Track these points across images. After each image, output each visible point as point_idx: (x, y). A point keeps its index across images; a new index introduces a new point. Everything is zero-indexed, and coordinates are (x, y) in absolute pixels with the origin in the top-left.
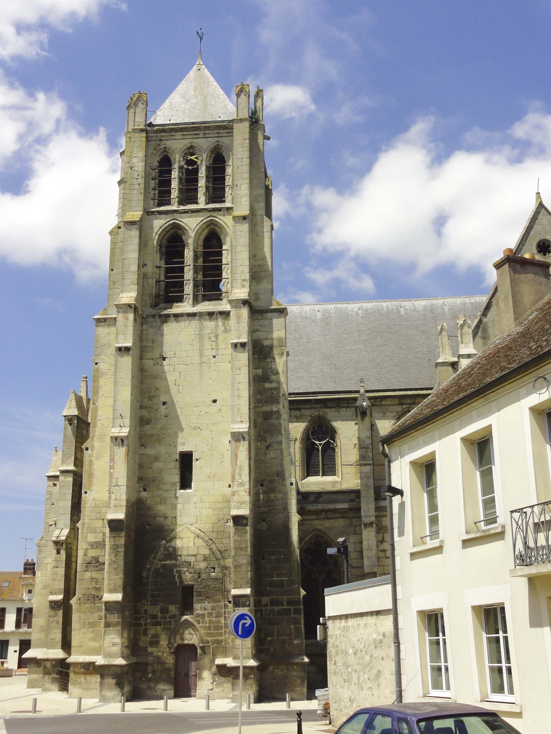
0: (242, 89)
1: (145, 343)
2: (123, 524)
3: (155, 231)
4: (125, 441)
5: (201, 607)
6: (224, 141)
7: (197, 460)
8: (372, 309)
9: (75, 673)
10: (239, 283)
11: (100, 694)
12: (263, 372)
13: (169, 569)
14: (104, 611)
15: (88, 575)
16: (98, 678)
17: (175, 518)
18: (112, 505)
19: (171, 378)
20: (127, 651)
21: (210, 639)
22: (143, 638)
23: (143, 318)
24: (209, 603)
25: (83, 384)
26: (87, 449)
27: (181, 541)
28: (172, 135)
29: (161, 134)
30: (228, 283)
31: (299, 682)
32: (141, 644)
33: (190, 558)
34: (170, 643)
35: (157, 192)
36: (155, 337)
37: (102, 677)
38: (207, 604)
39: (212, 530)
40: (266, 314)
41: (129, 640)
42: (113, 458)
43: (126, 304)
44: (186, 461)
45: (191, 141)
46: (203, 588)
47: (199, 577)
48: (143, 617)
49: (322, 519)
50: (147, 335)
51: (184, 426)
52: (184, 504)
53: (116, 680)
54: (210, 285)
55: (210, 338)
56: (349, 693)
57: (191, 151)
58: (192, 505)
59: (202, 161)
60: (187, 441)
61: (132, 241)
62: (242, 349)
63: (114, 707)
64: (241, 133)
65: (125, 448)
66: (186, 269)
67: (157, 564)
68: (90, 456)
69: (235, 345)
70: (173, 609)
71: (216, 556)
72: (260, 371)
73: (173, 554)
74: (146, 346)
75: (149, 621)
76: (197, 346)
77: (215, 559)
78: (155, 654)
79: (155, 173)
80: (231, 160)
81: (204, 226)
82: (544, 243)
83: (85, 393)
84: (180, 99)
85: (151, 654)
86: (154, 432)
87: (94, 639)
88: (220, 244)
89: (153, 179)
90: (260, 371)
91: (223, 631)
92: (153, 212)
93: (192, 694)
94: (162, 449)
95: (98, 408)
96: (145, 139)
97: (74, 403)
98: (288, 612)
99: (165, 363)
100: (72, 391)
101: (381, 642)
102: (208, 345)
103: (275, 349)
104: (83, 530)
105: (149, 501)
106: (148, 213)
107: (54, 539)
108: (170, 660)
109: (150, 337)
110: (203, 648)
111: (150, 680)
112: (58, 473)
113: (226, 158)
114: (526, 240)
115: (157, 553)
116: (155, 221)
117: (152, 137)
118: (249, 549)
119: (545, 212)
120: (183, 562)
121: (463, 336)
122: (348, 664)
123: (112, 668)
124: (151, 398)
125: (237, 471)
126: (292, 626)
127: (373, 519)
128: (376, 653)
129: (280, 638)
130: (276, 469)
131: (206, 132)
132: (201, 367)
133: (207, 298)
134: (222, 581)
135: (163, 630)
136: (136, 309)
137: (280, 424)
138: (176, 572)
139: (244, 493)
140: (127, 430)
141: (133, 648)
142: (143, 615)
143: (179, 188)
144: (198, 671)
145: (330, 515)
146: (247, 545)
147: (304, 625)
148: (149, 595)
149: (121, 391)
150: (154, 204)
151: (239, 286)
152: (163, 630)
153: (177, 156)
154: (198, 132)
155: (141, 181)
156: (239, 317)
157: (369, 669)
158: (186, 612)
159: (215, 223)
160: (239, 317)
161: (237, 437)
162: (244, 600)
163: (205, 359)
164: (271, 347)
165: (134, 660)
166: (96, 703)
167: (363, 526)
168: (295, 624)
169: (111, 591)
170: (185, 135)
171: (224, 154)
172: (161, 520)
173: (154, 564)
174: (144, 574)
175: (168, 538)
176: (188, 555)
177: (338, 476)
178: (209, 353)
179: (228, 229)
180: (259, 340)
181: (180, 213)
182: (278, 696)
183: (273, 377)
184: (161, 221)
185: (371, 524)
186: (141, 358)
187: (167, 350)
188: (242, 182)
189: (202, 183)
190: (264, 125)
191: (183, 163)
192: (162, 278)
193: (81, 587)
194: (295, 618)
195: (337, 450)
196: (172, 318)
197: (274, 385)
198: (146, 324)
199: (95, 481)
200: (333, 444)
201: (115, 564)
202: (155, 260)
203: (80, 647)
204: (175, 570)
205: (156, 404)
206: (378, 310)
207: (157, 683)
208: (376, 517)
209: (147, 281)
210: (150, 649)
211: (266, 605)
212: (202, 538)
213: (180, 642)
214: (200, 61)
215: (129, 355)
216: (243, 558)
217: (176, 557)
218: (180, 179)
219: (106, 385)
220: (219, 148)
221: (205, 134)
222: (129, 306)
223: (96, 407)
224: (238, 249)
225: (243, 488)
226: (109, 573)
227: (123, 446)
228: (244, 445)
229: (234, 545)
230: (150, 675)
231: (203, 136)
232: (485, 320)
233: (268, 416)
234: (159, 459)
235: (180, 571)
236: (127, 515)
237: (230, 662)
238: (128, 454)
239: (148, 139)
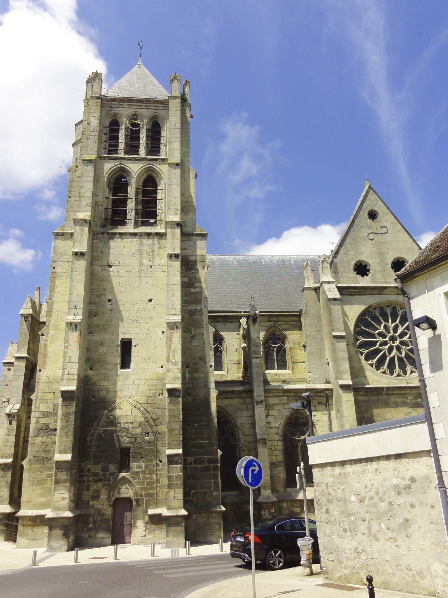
0: (175, 77)
1: (95, 254)
2: (74, 395)
3: (106, 171)
4: (78, 326)
6: (161, 113)
7: (136, 346)
8: (243, 260)
9: (23, 525)
10: (173, 211)
11: (48, 544)
12: (189, 280)
13: (111, 434)
14: (54, 470)
15: (39, 439)
16: (46, 530)
17: (116, 392)
18: (65, 379)
19: (115, 281)
20: (73, 505)
21: (143, 493)
22: (85, 493)
23: (94, 234)
24: (143, 462)
25: (37, 293)
26: (43, 335)
27: (120, 411)
28: (121, 105)
29: (113, 103)
30: (162, 214)
31: (217, 527)
32: (84, 498)
33: (128, 425)
35: (107, 144)
36: (103, 249)
37: (50, 529)
38: (141, 463)
39: (146, 402)
40: (191, 237)
41: (74, 494)
42: (68, 340)
43: (82, 220)
44: (126, 346)
45: (135, 110)
46: (139, 449)
47: (135, 441)
48: (86, 475)
49: (223, 398)
50: (97, 247)
51: (124, 320)
52: (124, 380)
53: (63, 531)
54: (148, 212)
55: (147, 253)
56: (354, 544)
57: (135, 117)
59: (143, 125)
60: (127, 331)
61: (88, 174)
62: (176, 259)
63: (64, 558)
64: (175, 106)
65: (78, 331)
66: (129, 201)
67: (100, 430)
69: (170, 256)
70: (113, 468)
71: (150, 424)
72: (187, 279)
73: (113, 422)
74: (96, 256)
75: (91, 478)
76: (137, 258)
77: (149, 426)
78: (96, 506)
79: (107, 130)
80: (166, 126)
81: (144, 171)
82: (372, 213)
83: (38, 299)
84: (126, 84)
85: (92, 507)
86: (100, 323)
87: (41, 495)
88: (155, 185)
89: (105, 134)
90: (187, 279)
91: (155, 486)
92: (105, 157)
93: (126, 540)
94: (107, 336)
96: (100, 104)
97: (29, 305)
98: (208, 469)
99: (110, 269)
100: (28, 295)
101: (409, 487)
102: (146, 258)
103: (198, 263)
104: (36, 400)
105: (94, 378)
106: (100, 157)
107: (7, 412)
108: (109, 511)
109: (99, 249)
110: (137, 501)
111: (90, 530)
112: (13, 360)
113: (161, 125)
114: (361, 209)
115: (100, 421)
116: (106, 164)
117: (105, 104)
118: (181, 416)
119: (373, 192)
120: (122, 428)
121: (324, 269)
122: (350, 512)
123: (61, 520)
124: (98, 296)
126: (212, 481)
127: (263, 398)
128: (400, 500)
129: (202, 490)
130: (199, 354)
131: (147, 104)
132: (140, 274)
133: (145, 223)
134: (154, 444)
135: (104, 486)
136: (90, 224)
137: (203, 320)
138: (116, 436)
139: (177, 371)
140: (81, 318)
141: (78, 502)
142: (86, 473)
143: (125, 143)
144: (133, 520)
145: (229, 395)
146: (180, 413)
147: (222, 479)
148: (92, 456)
150: (105, 152)
151: (173, 213)
152: (104, 486)
153: (125, 120)
154: (141, 104)
155: (96, 133)
156: (173, 235)
157: (389, 517)
158: (123, 470)
159: (153, 169)
160: (173, 235)
161: (172, 326)
162: (177, 458)
163: (143, 268)
164: (195, 262)
165: (78, 512)
166: (44, 552)
167: (255, 404)
168: (214, 479)
169: (61, 452)
170: (131, 105)
171: (160, 122)
172: (105, 393)
173: (97, 430)
174: (89, 439)
176: (127, 423)
177: (224, 371)
178: (147, 263)
179: (162, 175)
180: (186, 256)
181: (126, 160)
182: (200, 540)
183: (197, 284)
184: (111, 164)
185: (261, 402)
186: (92, 265)
187: (112, 259)
188: (175, 140)
189: (143, 140)
190: (190, 104)
191: (128, 125)
192: (110, 206)
193: (32, 450)
194: (214, 473)
195: (223, 352)
196: (118, 236)
197: (198, 290)
198: (97, 239)
200: (221, 348)
202: (105, 193)
203: (29, 502)
204: (115, 435)
205: (103, 301)
206: (247, 261)
207: (97, 532)
208: (265, 397)
210: (91, 503)
211: (191, 464)
213: (118, 496)
214: (140, 62)
215: (83, 259)
217: (116, 424)
218: (126, 136)
219: (62, 285)
220: (156, 117)
221: (146, 106)
222: (85, 221)
223: (52, 302)
224: (172, 187)
225: (176, 367)
226: (61, 436)
227: (76, 330)
228: (177, 333)
229: (169, 413)
230: (91, 525)
231: (145, 108)
232: (335, 260)
233: (192, 313)
234: (104, 343)
235: (119, 435)
236: (78, 387)
237: (165, 512)
238: (80, 337)
239: (102, 106)
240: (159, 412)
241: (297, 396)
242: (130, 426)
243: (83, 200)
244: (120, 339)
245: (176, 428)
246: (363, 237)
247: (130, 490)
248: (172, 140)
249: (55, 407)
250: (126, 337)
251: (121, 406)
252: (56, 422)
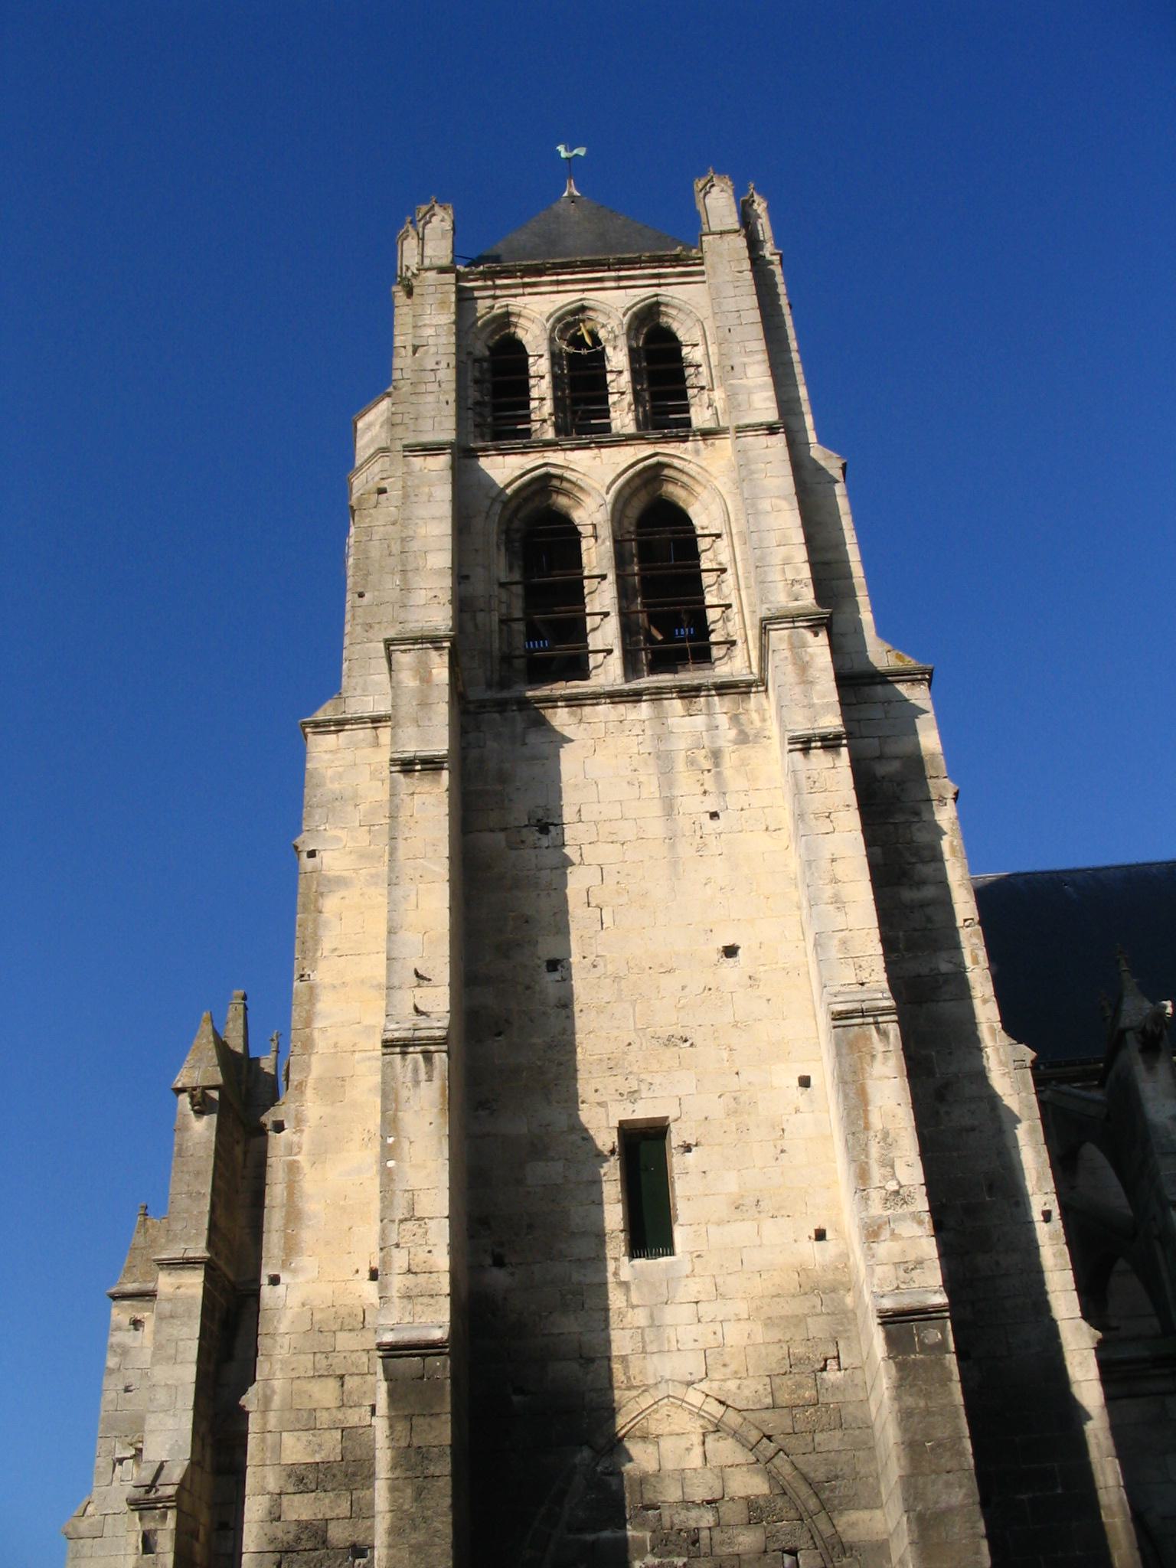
7: (688, 1148)
26: (279, 1127)
33: (694, 1513)
44: (645, 1147)
54: (672, 626)
55: (691, 762)
58: (686, 1312)
60: (644, 1087)
68: (290, 1148)
76: (652, 787)
81: (638, 481)
95: (318, 991)
102: (686, 783)
118: (968, 1444)
125: (875, 1150)
149: (413, 899)
170: (565, 282)
176: (687, 1504)
178: (693, 804)
183: (926, 870)
197: (929, 892)
199: (307, 1236)
201: (415, 1528)
209: (474, 618)
216: (948, 1485)
224: (765, 505)
228: (886, 1059)
240: (836, 1445)
242: (707, 1518)
243: (417, 581)
244: (606, 1139)
245: (950, 1510)
248: (737, 361)
249: (348, 1444)
250: (642, 1111)
251: (654, 1428)
252: (362, 1512)
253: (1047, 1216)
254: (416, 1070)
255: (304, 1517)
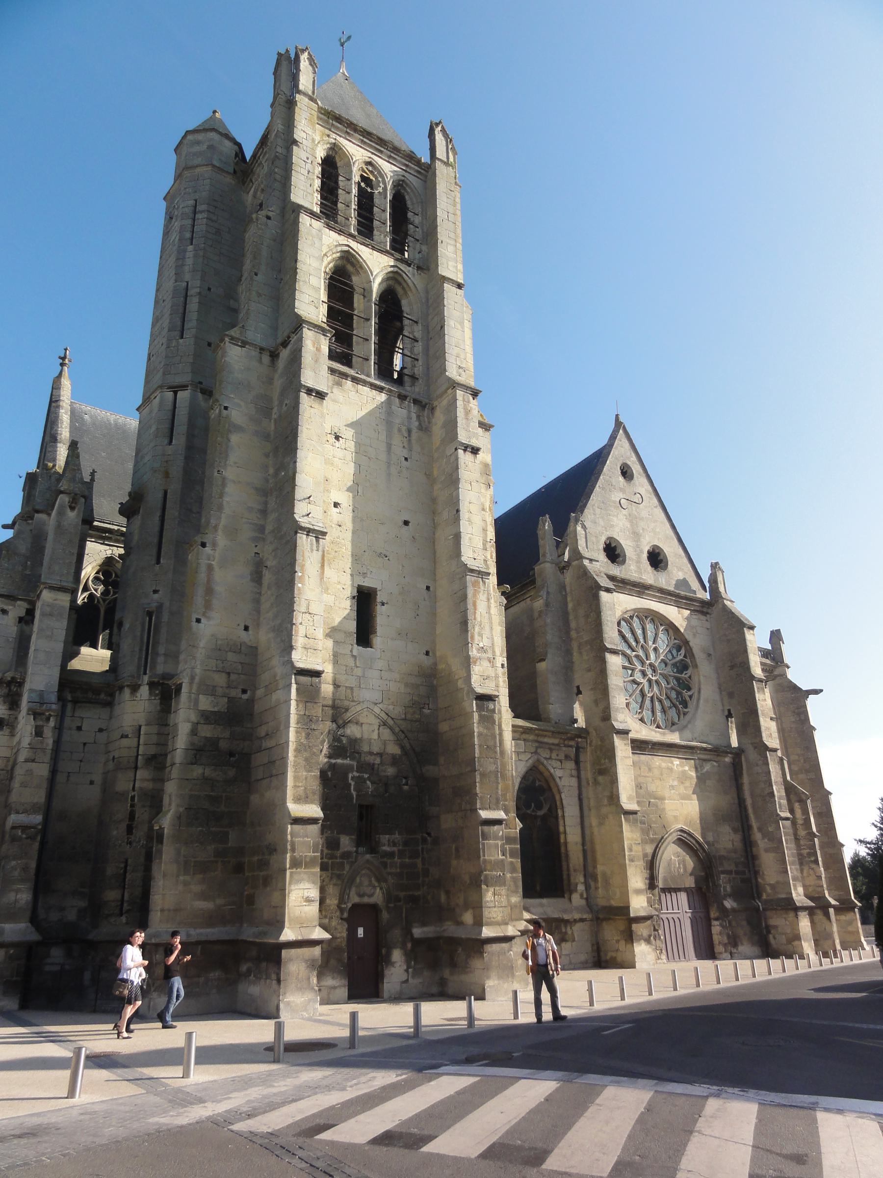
5: (389, 840)
7: (383, 604)
21: (402, 894)
28: (348, 133)
33: (373, 757)
34: (342, 900)
55: (399, 430)
60: (369, 573)
87: (203, 896)
135: (331, 878)
138: (353, 778)
169: (298, 800)
171: (407, 197)
175: (341, 722)
176: (371, 753)
201: (305, 750)
204: (350, 775)
212: (391, 728)
220: (402, 185)
241: (538, 742)
246: (614, 502)
247: (378, 890)
253: (503, 665)
254: (312, 544)
255: (208, 735)
